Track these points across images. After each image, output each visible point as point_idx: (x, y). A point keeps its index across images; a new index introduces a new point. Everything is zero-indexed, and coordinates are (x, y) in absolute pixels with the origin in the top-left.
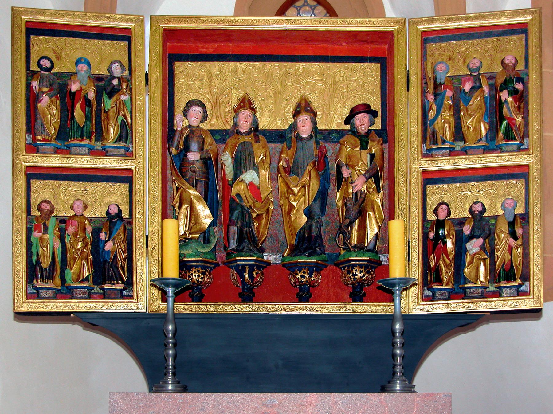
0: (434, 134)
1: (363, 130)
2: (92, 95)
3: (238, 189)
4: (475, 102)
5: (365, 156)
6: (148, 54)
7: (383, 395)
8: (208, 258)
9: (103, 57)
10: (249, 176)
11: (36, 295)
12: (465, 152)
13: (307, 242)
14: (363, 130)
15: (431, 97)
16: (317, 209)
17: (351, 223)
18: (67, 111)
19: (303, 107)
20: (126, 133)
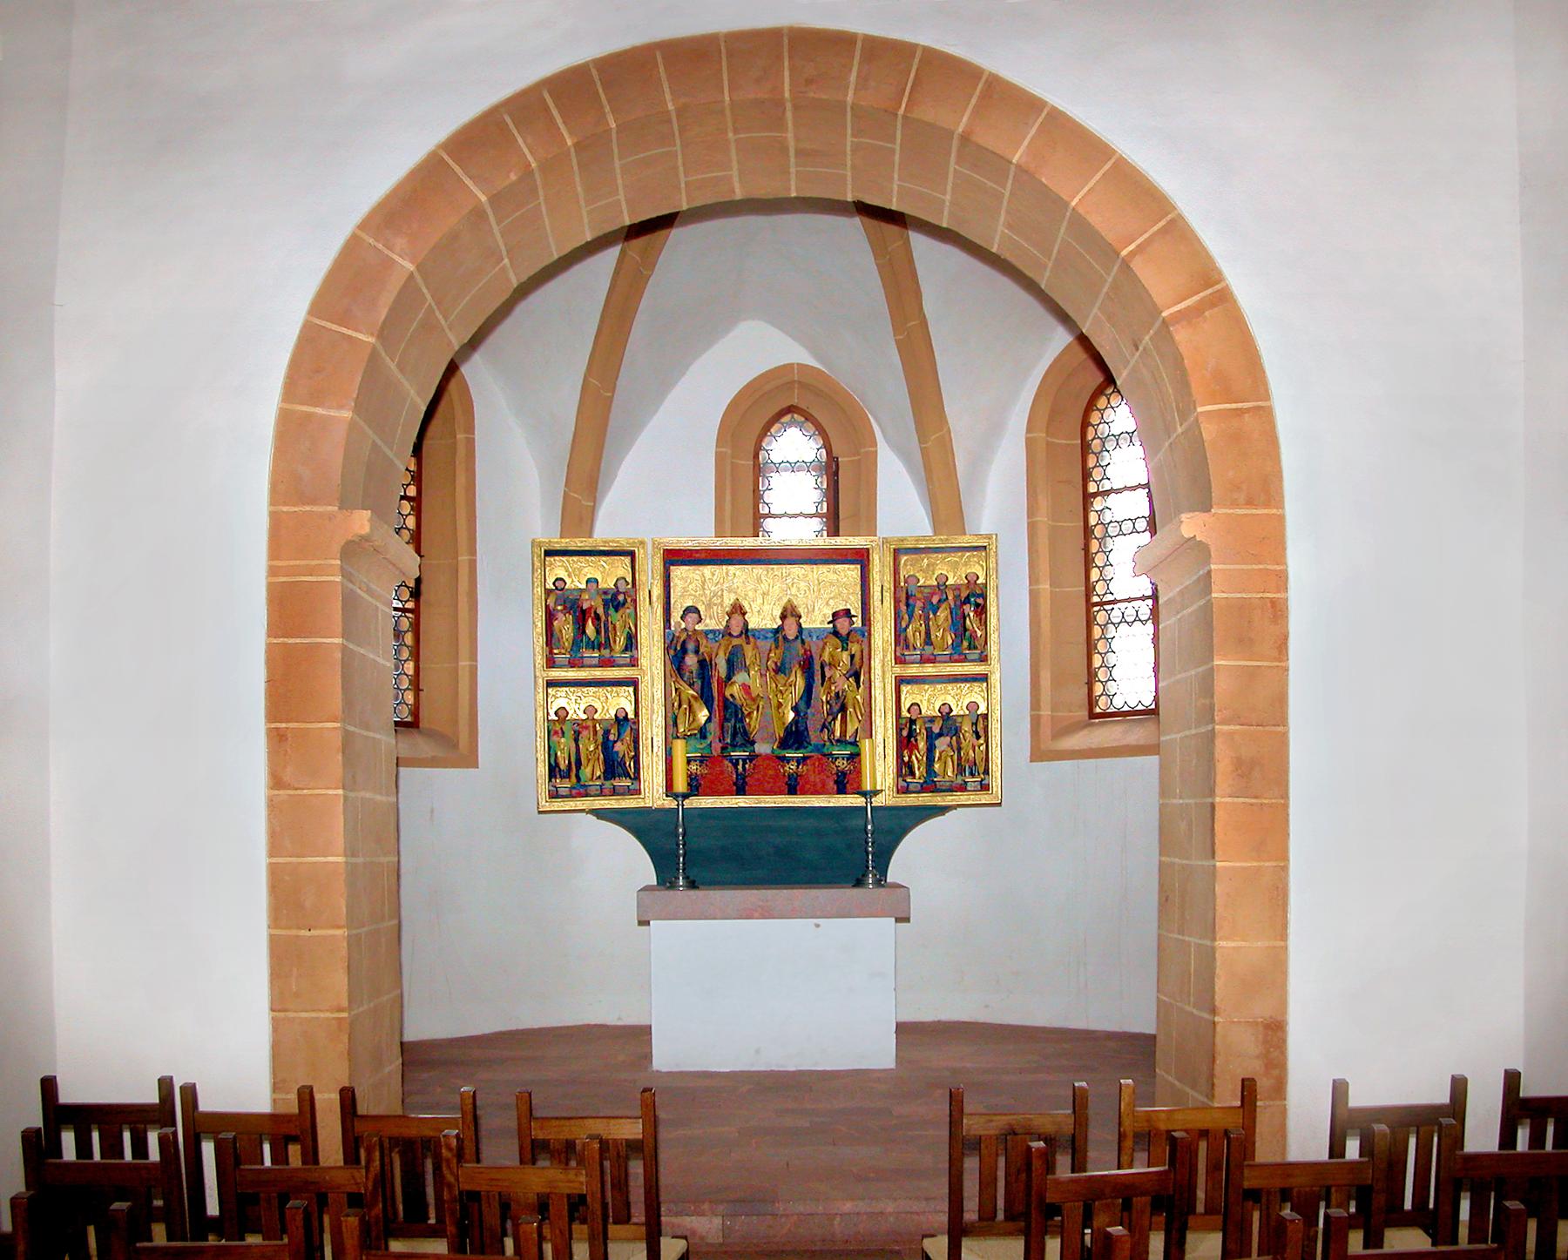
0: (906, 639)
1: (844, 632)
2: (600, 611)
3: (734, 690)
4: (943, 614)
5: (845, 656)
6: (650, 566)
7: (856, 891)
8: (706, 752)
9: (609, 574)
10: (740, 677)
11: (554, 795)
12: (932, 660)
13: (795, 736)
14: (844, 632)
15: (903, 607)
16: (802, 706)
17: (834, 719)
19: (789, 612)
20: (631, 642)
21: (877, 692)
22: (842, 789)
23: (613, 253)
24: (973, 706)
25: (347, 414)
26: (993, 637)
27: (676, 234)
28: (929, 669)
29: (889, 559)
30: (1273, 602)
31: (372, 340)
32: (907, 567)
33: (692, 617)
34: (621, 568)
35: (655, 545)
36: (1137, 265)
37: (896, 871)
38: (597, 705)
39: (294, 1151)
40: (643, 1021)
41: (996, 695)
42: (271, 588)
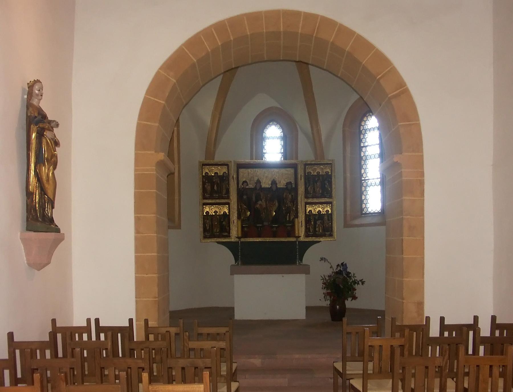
2: (219, 182)
9: (221, 171)
10: (260, 202)
18: (212, 187)
20: (228, 192)
21: (299, 207)
22: (289, 236)
23: (222, 76)
24: (327, 211)
25: (157, 124)
26: (334, 191)
27: (239, 68)
28: (315, 200)
29: (303, 167)
30: (420, 180)
31: (163, 102)
32: (309, 170)
33: (245, 184)
34: (225, 170)
35: (234, 162)
36: (381, 81)
37: (305, 261)
38: (217, 210)
39: (48, 353)
40: (232, 306)
41: (334, 208)
42: (135, 175)
